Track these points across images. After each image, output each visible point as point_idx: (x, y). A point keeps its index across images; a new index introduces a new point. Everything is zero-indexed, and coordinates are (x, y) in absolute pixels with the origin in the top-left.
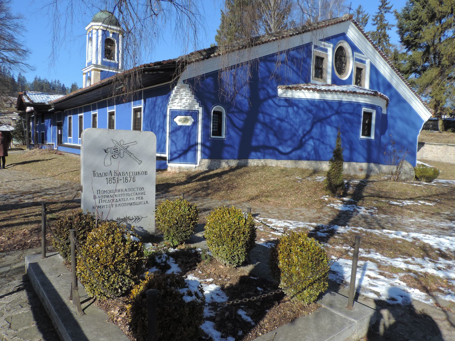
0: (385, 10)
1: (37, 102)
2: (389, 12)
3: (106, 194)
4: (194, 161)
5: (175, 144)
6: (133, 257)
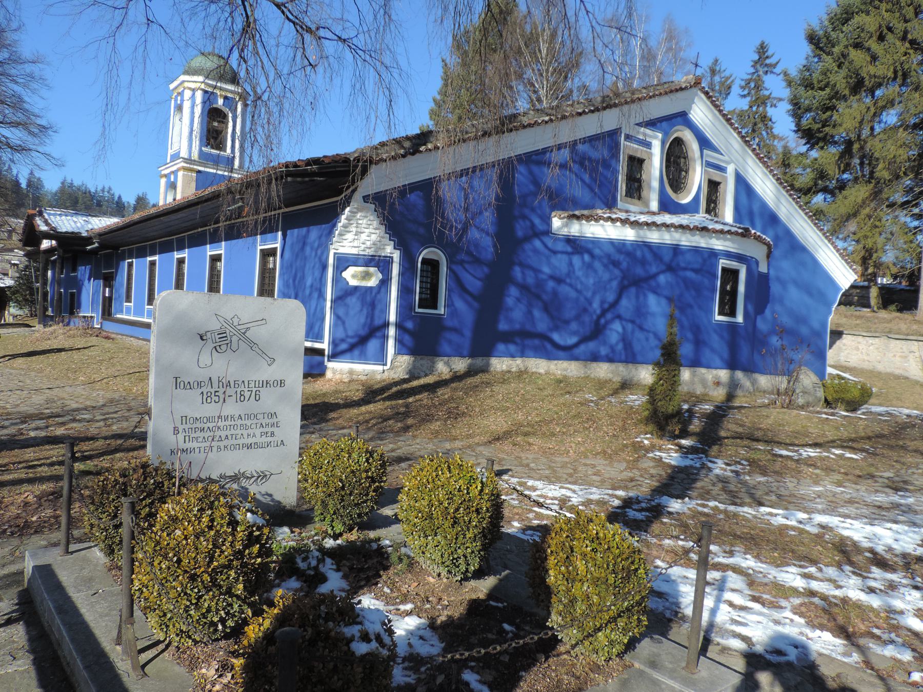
0: (766, 69)
1: (64, 230)
2: (772, 72)
3: (198, 425)
4: (381, 358)
5: (344, 323)
6: (251, 558)
